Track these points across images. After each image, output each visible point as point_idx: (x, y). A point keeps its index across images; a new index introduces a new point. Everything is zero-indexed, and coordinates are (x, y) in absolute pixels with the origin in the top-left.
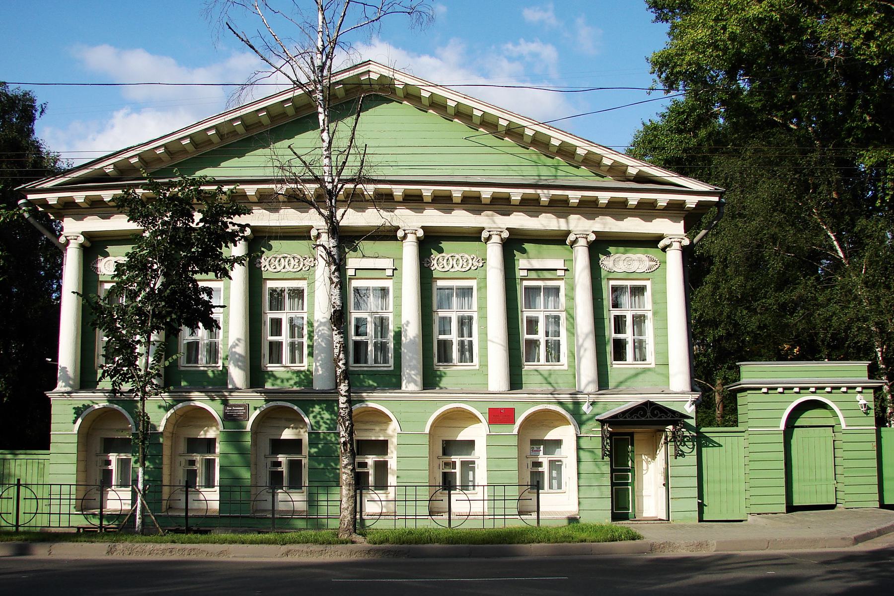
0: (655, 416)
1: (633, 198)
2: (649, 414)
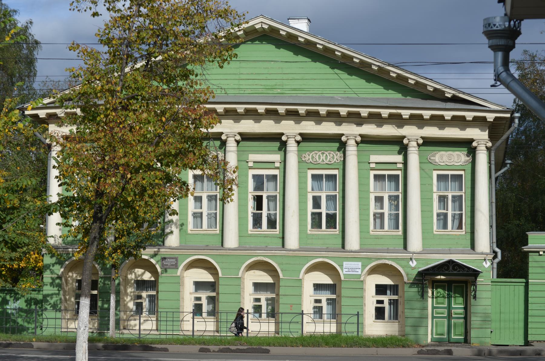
0: (456, 270)
1: (448, 115)
2: (451, 268)
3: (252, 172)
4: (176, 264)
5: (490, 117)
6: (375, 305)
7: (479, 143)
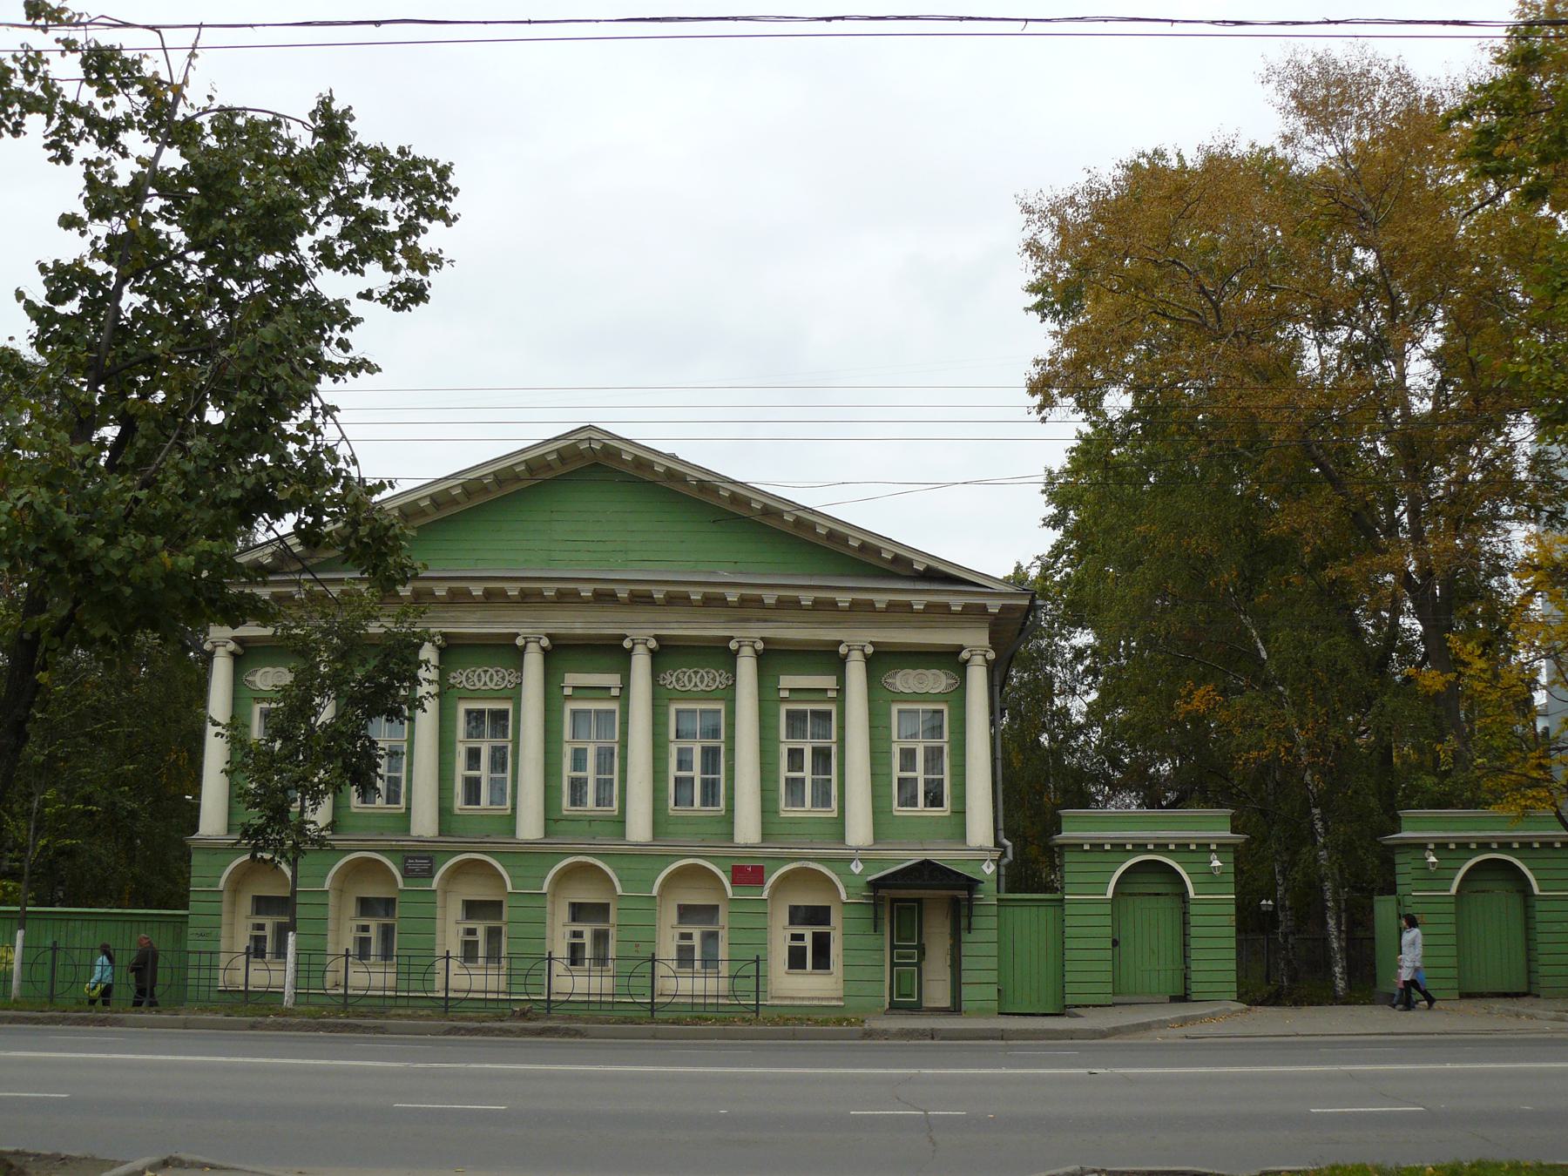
3: (784, 709)
4: (431, 868)
6: (789, 942)
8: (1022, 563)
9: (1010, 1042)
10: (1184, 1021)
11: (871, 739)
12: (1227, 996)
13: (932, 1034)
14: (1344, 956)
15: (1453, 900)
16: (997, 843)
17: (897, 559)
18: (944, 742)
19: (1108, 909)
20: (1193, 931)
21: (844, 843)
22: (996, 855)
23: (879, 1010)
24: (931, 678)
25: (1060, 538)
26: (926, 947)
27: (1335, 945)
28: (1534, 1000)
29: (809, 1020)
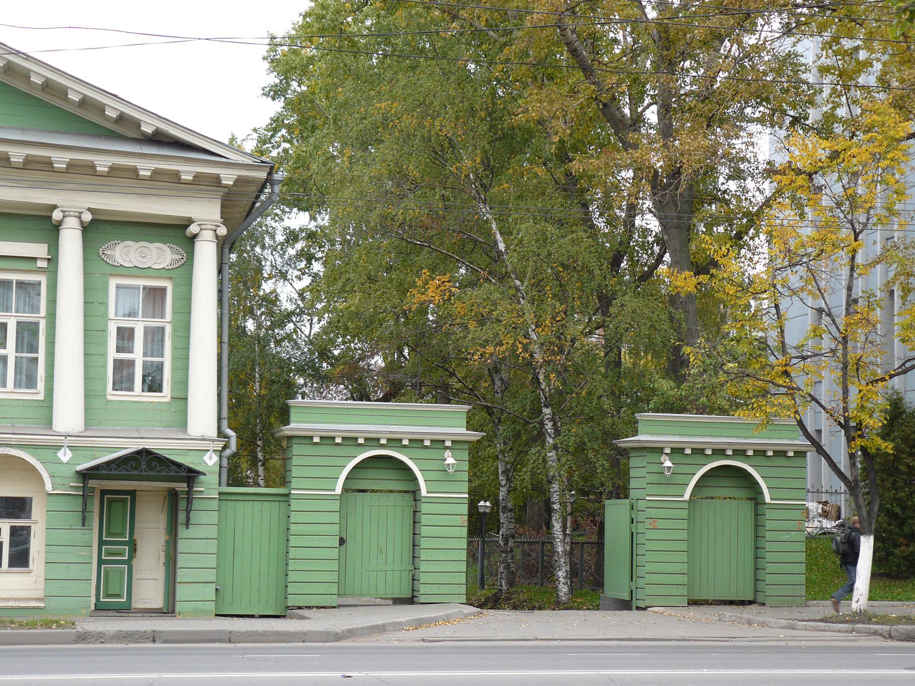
0: (152, 469)
2: (143, 466)
5: (228, 177)
7: (203, 227)
8: (236, 135)
9: (238, 645)
10: (418, 624)
11: (85, 316)
12: (455, 599)
13: (154, 637)
14: (568, 561)
15: (686, 505)
16: (220, 433)
17: (122, 118)
18: (167, 321)
19: (336, 506)
20: (424, 531)
21: (51, 428)
22: (219, 445)
23: (84, 612)
24: (155, 252)
25: (280, 110)
26: (138, 543)
27: (560, 549)
28: (762, 609)
29: (12, 622)
